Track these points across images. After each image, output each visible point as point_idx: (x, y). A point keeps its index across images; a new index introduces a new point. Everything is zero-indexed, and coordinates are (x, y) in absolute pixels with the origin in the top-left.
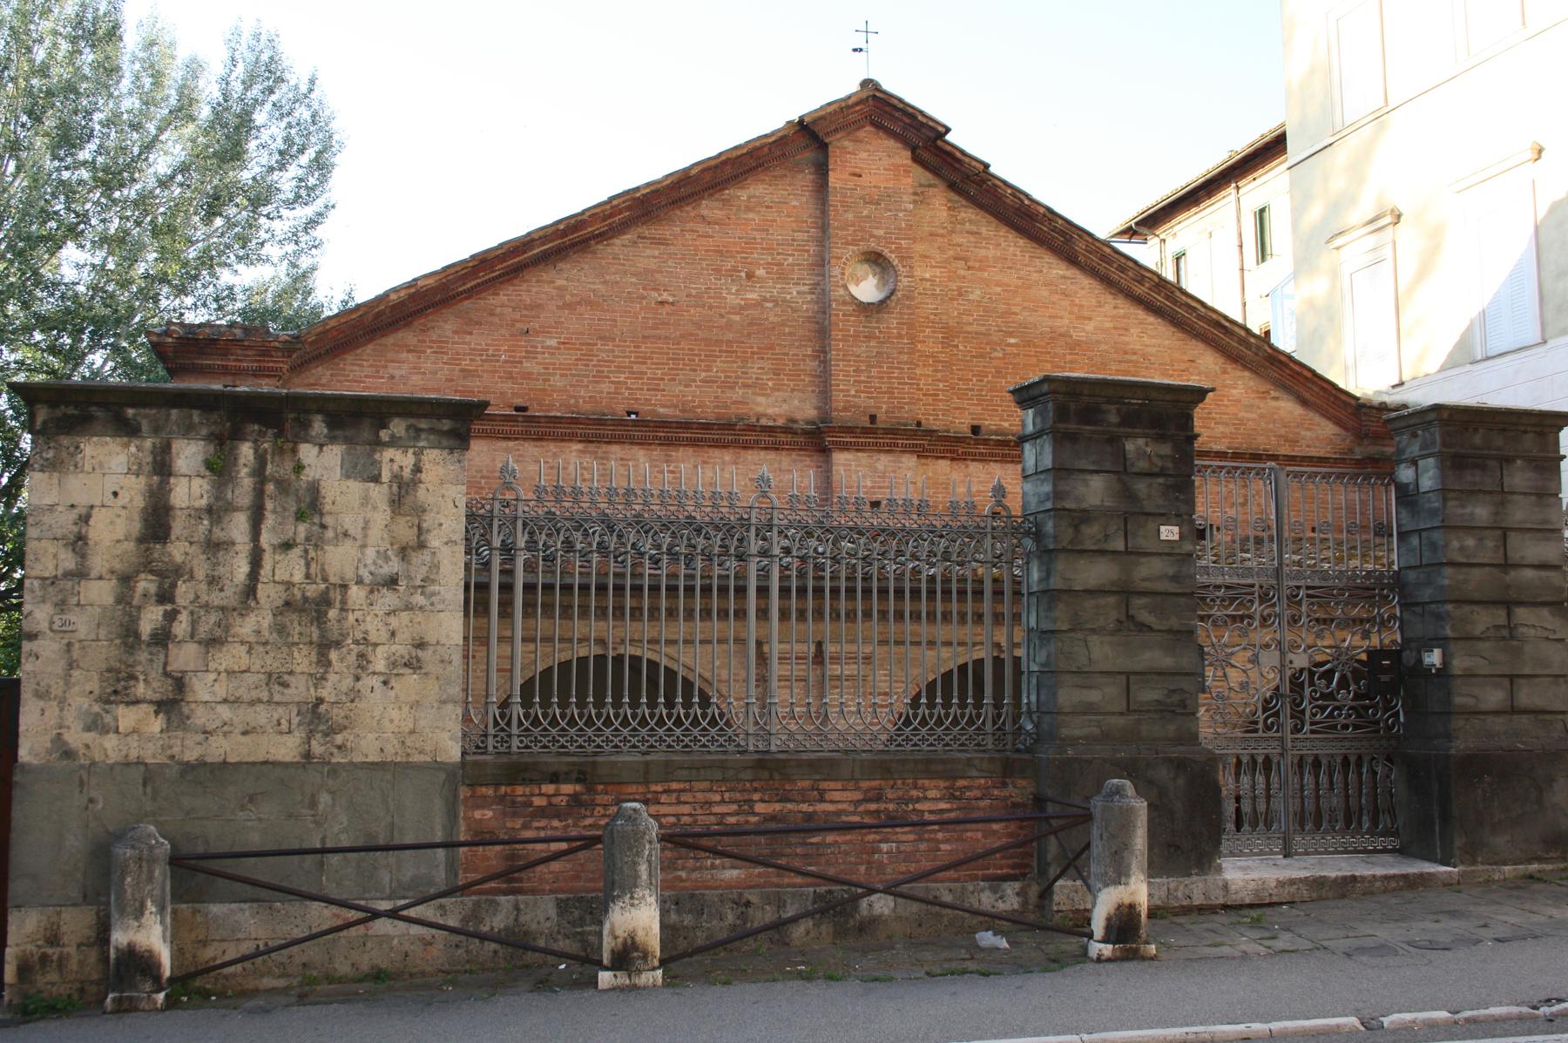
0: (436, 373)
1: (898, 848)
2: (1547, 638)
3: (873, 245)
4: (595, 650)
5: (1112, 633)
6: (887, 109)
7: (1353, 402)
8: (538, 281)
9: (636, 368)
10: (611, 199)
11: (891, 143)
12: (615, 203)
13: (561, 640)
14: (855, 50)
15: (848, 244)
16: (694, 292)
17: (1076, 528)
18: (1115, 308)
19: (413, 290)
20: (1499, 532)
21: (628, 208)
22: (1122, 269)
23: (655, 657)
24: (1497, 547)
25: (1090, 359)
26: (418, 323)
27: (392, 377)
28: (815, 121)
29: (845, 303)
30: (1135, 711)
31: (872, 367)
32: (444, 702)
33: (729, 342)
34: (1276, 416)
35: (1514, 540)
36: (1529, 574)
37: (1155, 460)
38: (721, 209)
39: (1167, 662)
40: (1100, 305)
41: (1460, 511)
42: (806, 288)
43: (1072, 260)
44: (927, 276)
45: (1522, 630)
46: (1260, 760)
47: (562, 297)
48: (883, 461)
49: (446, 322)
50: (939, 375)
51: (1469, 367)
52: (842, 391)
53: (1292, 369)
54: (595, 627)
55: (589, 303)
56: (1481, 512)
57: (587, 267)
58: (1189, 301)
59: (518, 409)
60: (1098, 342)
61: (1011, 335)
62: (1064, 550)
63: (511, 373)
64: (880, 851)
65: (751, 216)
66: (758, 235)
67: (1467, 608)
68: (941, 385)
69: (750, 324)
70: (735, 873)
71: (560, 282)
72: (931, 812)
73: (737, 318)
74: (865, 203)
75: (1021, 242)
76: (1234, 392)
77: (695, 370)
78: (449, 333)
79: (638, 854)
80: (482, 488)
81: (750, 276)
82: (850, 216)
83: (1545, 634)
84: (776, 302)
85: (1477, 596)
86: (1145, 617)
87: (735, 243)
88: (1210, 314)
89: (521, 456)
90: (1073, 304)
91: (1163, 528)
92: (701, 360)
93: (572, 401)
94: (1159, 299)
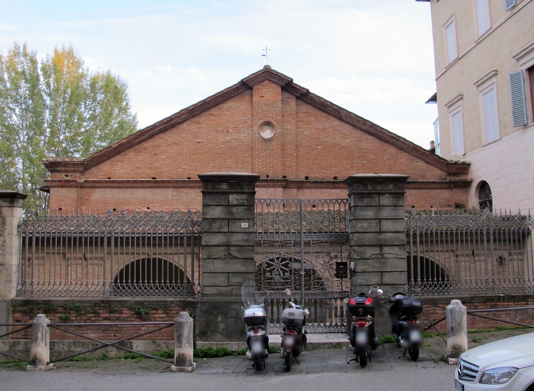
0: (128, 168)
1: (147, 329)
2: (397, 258)
3: (268, 119)
4: (147, 257)
5: (223, 259)
6: (272, 75)
7: (445, 162)
8: (159, 138)
9: (190, 164)
10: (181, 111)
11: (274, 86)
12: (182, 112)
13: (137, 254)
14: (263, 55)
15: (259, 119)
16: (209, 138)
17: (210, 225)
18: (357, 134)
19: (119, 143)
20: (378, 220)
21: (187, 113)
22: (358, 121)
23: (166, 259)
24: (377, 226)
25: (348, 152)
26: (122, 154)
27: (115, 170)
28: (247, 81)
29: (258, 139)
30: (231, 285)
31: (268, 159)
32: (7, 282)
33: (220, 154)
34: (417, 168)
35: (383, 222)
36: (390, 235)
37: (240, 200)
38: (218, 111)
39: (243, 269)
40: (351, 133)
41: (361, 213)
42: (246, 135)
43: (341, 119)
44: (289, 128)
45: (386, 255)
46: (275, 301)
47: (167, 142)
48: (271, 190)
49: (131, 152)
50: (293, 161)
51: (481, 148)
52: (257, 168)
53: (421, 152)
54: (146, 249)
55: (176, 144)
56: (370, 213)
57: (174, 132)
58: (383, 130)
59: (153, 178)
60: (351, 146)
61: (319, 145)
62: (206, 232)
63: (151, 167)
64: (141, 330)
65: (228, 112)
66: (230, 119)
67: (364, 248)
68: (294, 164)
69: (227, 148)
70: (94, 335)
71: (166, 138)
72: (159, 318)
73: (223, 146)
74: (265, 106)
75: (323, 114)
76: (401, 160)
77: (209, 163)
78: (132, 156)
79: (38, 330)
80: (142, 203)
81: (227, 132)
82: (260, 110)
83: (396, 256)
84: (236, 140)
85: (368, 244)
86: (235, 254)
87: (223, 122)
88: (391, 134)
89: (154, 193)
90: (341, 134)
91: (242, 224)
92: (211, 160)
93: (170, 175)
94: (372, 130)
